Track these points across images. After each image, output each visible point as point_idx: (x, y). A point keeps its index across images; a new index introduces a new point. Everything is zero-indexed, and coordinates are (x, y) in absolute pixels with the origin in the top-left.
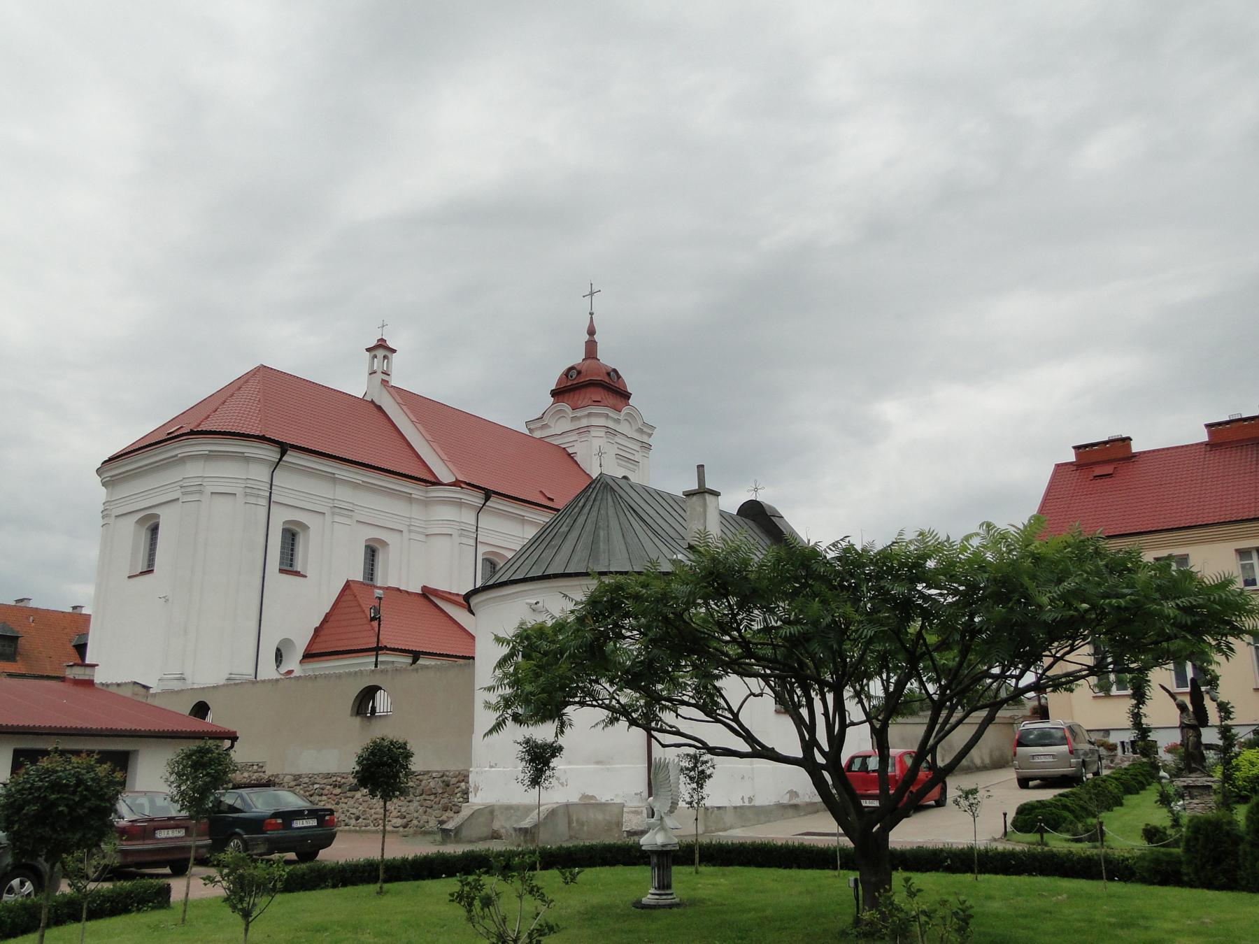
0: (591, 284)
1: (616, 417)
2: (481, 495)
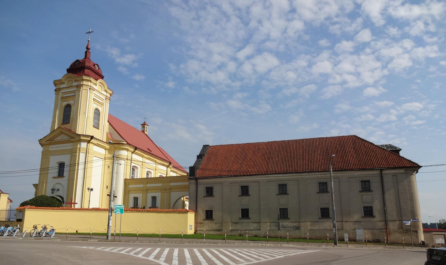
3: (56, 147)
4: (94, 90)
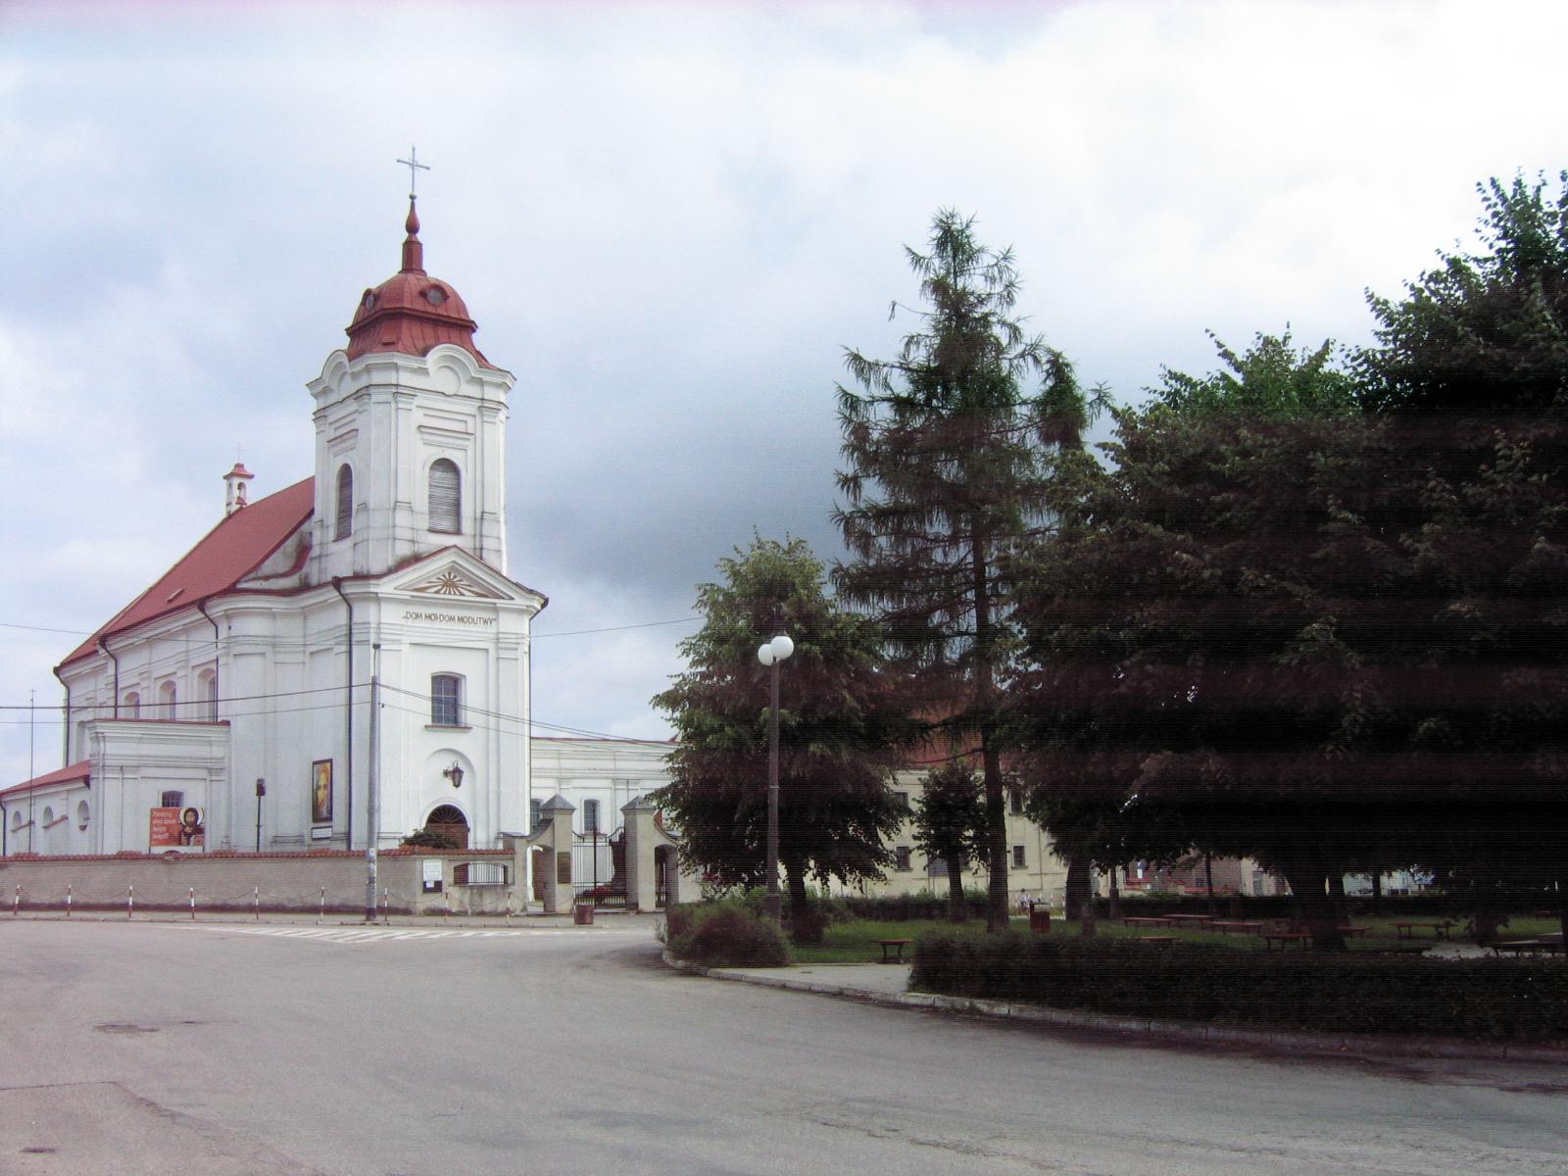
0: (414, 150)
1: (415, 365)
2: (195, 609)
4: (413, 392)
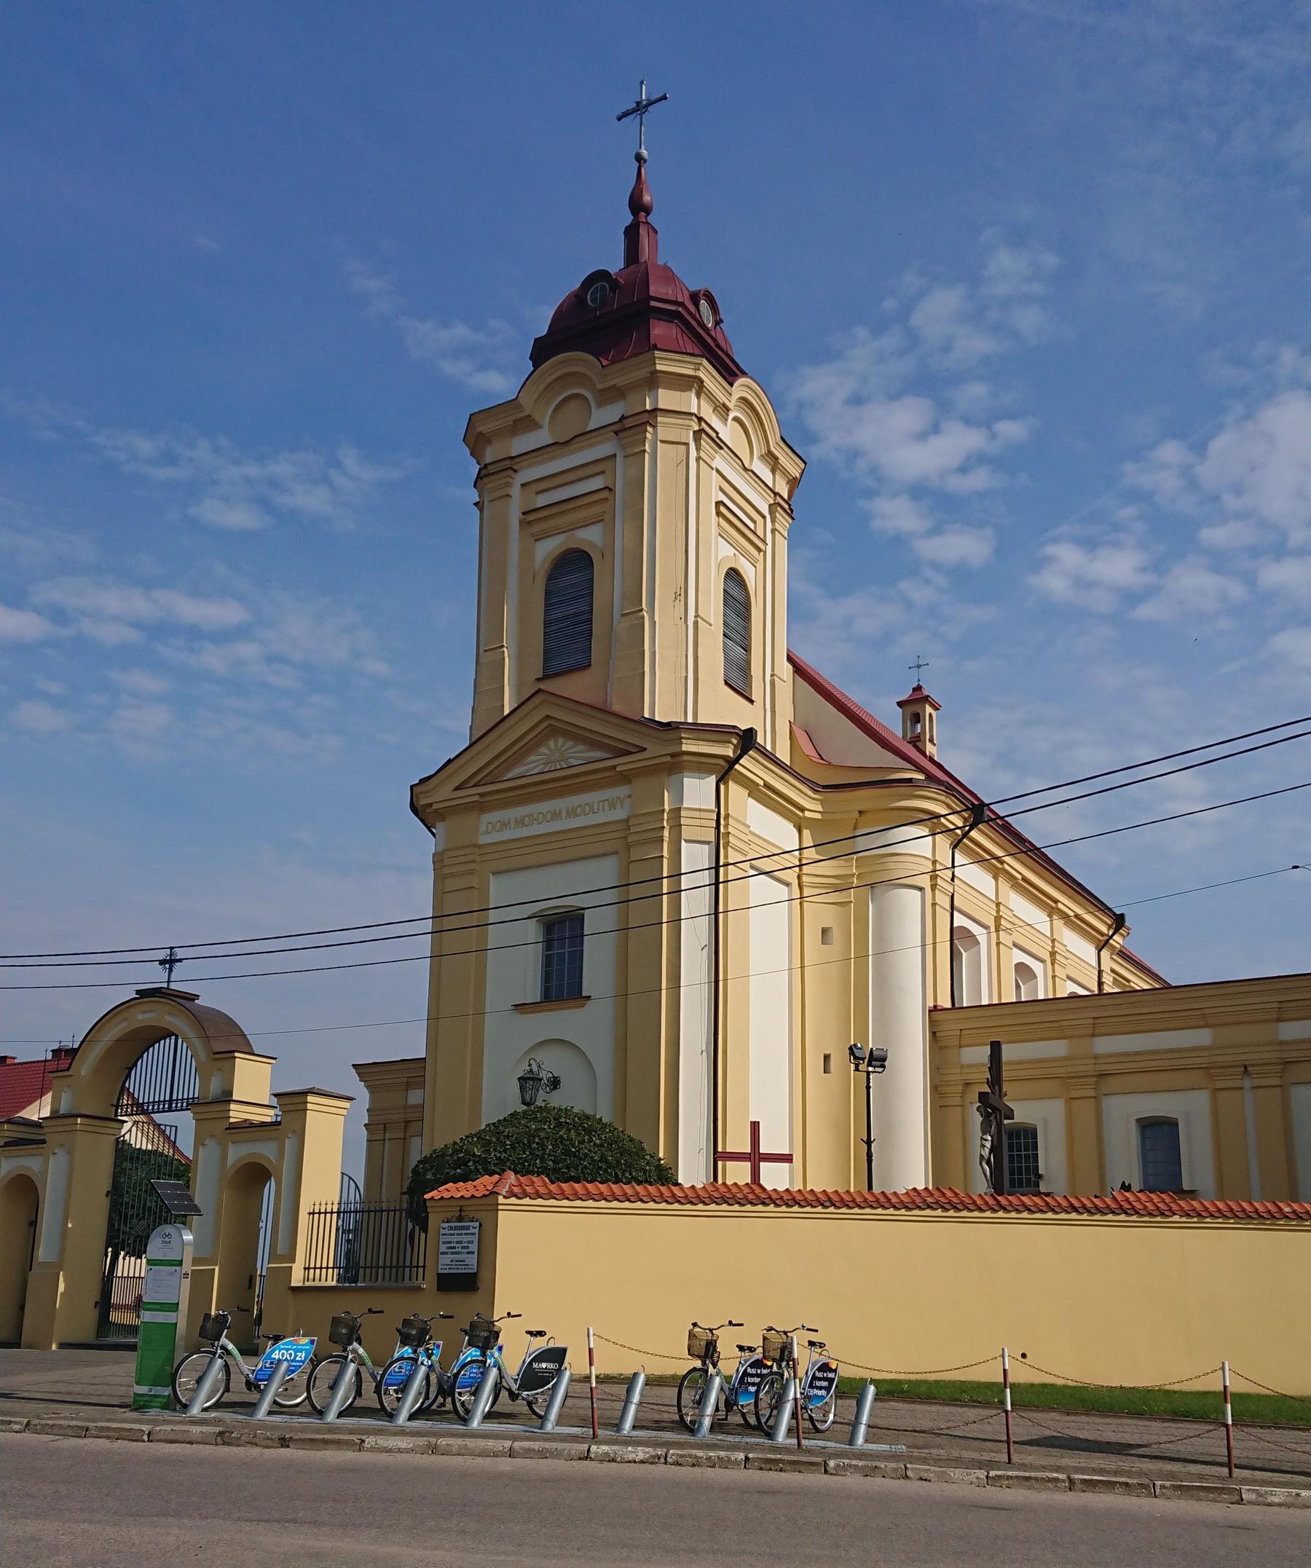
3: (521, 823)
